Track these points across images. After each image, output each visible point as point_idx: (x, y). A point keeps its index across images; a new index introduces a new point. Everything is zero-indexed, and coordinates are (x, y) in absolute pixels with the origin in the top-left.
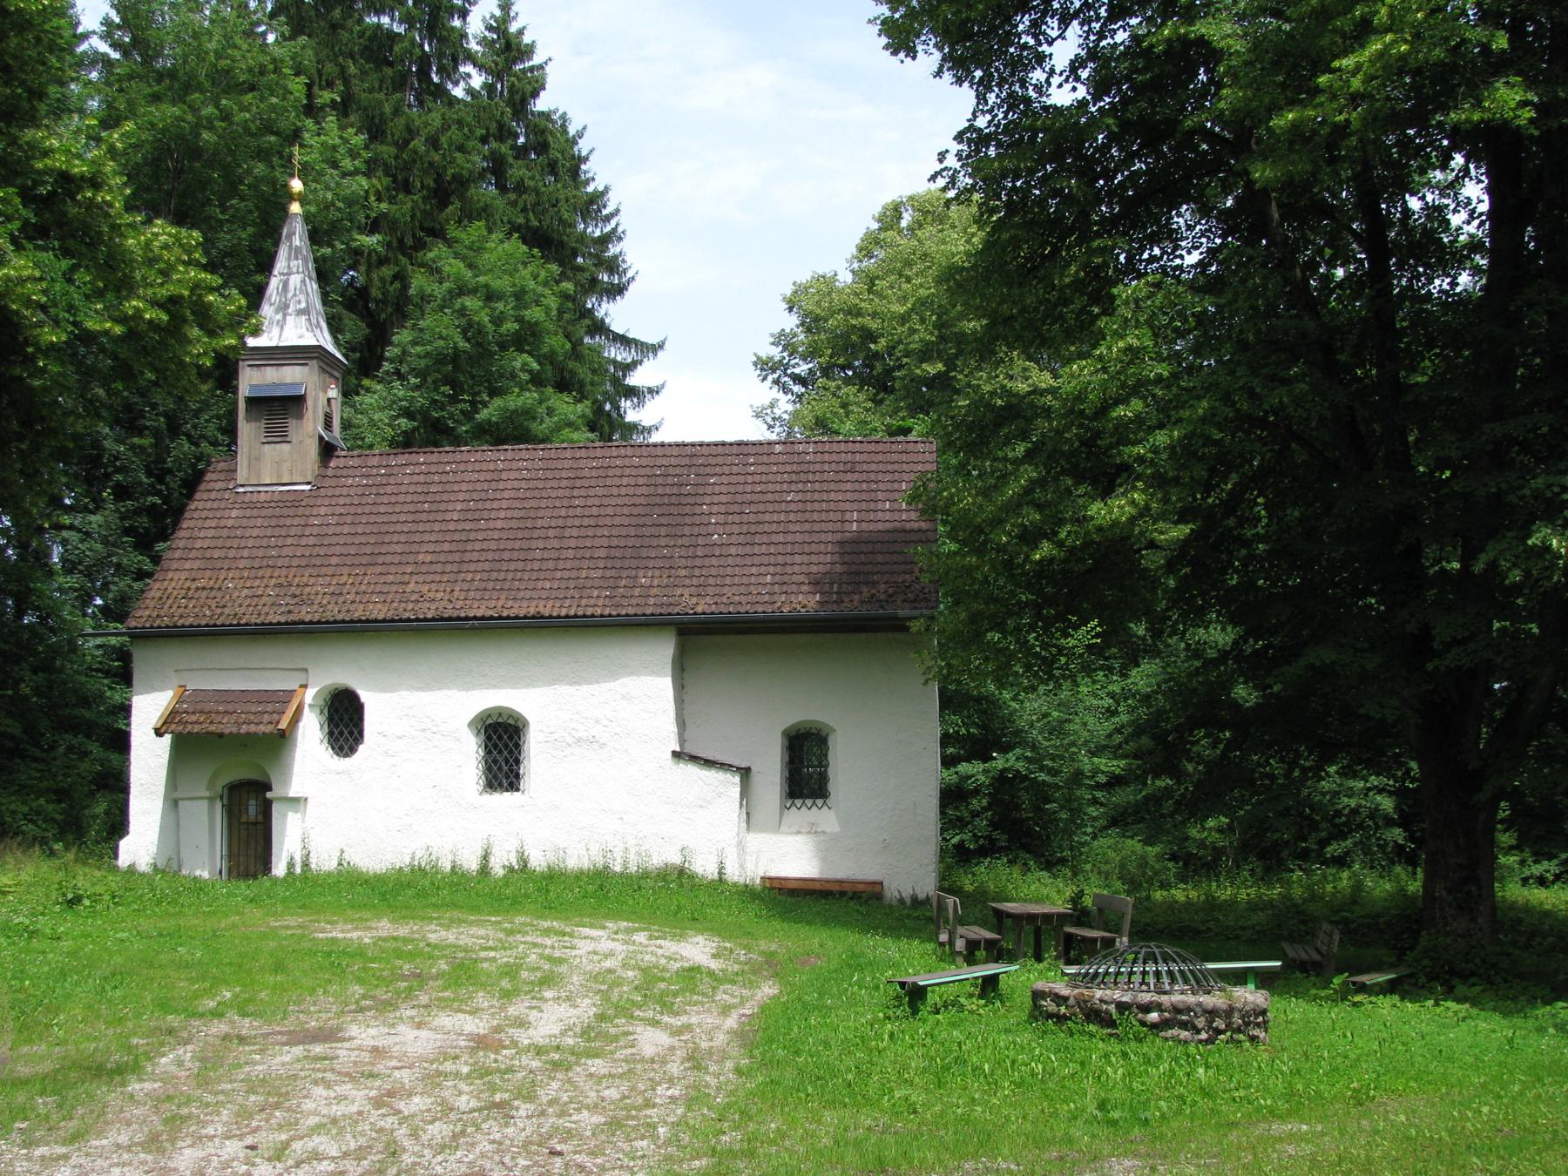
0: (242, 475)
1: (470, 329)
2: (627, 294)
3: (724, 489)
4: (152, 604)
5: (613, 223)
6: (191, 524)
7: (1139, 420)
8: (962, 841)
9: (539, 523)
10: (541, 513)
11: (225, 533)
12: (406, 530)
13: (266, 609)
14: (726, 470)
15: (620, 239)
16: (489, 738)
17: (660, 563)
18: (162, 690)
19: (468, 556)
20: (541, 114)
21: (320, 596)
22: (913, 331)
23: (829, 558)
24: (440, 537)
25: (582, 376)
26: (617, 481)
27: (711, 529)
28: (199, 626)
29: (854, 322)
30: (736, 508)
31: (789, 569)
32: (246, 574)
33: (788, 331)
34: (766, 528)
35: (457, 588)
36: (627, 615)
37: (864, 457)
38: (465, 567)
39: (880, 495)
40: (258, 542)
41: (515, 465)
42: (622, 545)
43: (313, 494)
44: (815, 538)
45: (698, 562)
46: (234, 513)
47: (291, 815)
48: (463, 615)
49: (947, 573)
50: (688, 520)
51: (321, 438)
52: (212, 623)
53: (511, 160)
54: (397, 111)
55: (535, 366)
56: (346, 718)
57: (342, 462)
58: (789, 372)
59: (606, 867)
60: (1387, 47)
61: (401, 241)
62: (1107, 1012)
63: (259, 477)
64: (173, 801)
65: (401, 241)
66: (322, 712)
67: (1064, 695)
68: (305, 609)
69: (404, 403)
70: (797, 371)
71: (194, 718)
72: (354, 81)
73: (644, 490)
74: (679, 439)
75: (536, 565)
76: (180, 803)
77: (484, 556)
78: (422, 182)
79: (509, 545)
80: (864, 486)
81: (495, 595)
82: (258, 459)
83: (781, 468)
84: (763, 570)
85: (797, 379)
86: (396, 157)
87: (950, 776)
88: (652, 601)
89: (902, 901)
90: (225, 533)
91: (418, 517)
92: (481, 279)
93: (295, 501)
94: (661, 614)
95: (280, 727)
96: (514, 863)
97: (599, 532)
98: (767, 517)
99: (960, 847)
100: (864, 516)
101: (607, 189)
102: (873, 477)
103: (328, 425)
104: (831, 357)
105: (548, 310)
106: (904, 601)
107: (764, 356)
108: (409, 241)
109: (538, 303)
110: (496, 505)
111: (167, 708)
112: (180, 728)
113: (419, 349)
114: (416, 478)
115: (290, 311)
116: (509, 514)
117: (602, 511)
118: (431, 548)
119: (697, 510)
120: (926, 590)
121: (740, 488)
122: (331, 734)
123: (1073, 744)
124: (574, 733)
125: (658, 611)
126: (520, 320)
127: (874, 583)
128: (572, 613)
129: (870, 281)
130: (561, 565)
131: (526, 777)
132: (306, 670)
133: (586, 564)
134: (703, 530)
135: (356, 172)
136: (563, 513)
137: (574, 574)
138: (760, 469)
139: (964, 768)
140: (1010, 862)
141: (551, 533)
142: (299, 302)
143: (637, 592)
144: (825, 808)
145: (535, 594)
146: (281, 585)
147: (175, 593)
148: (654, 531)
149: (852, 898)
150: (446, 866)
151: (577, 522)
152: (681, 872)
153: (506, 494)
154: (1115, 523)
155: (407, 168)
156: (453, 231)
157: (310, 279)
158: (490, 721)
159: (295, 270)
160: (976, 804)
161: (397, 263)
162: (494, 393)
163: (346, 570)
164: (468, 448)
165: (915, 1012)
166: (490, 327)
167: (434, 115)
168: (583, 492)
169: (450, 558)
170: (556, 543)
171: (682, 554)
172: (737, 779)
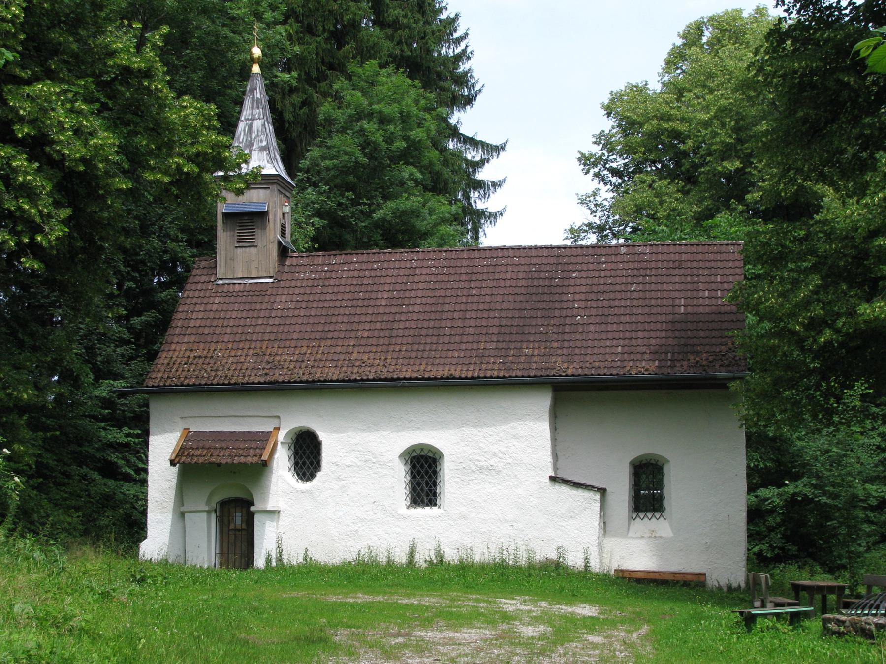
0: (221, 271)
1: (366, 145)
2: (476, 104)
3: (583, 281)
4: (163, 369)
6: (186, 308)
8: (761, 551)
9: (447, 308)
10: (447, 300)
11: (212, 315)
12: (347, 313)
13: (248, 372)
14: (585, 267)
15: (469, 58)
16: (413, 467)
17: (538, 338)
18: (171, 432)
19: (395, 333)
21: (287, 363)
22: (716, 134)
23: (664, 334)
25: (447, 176)
26: (502, 276)
27: (575, 312)
28: (200, 385)
29: (666, 126)
30: (593, 296)
31: (634, 342)
32: (230, 346)
33: (607, 132)
34: (616, 311)
35: (389, 357)
36: (516, 377)
37: (689, 257)
38: (393, 341)
39: (701, 286)
41: (425, 264)
42: (509, 324)
43: (275, 285)
44: (653, 318)
46: (217, 300)
47: (268, 523)
48: (395, 377)
49: (756, 349)
50: (557, 305)
51: (279, 243)
52: (209, 382)
55: (419, 176)
56: (301, 452)
58: (608, 166)
59: (503, 560)
61: (308, 74)
62: (870, 630)
63: (234, 273)
65: (308, 74)
66: (290, 448)
68: (277, 372)
69: (316, 205)
70: (614, 165)
71: (198, 452)
73: (523, 283)
75: (446, 340)
76: (186, 515)
77: (407, 333)
78: (324, 27)
79: (426, 324)
80: (689, 279)
81: (418, 362)
82: (232, 259)
83: (626, 266)
84: (615, 342)
85: (615, 172)
88: (534, 366)
89: (720, 588)
90: (212, 315)
91: (355, 303)
94: (541, 376)
95: (263, 458)
96: (433, 557)
97: (492, 314)
98: (617, 303)
99: (759, 555)
100: (689, 301)
101: (457, 16)
102: (695, 272)
103: (283, 234)
104: (644, 154)
105: (428, 131)
106: (721, 366)
108: (314, 74)
109: (420, 125)
110: (413, 294)
111: (177, 445)
112: (189, 459)
113: (328, 162)
114: (351, 274)
115: (254, 147)
116: (424, 301)
118: (367, 326)
119: (564, 298)
120: (737, 358)
121: (596, 281)
122: (296, 464)
123: (849, 474)
124: (477, 463)
125: (540, 373)
126: (406, 138)
127: (698, 352)
128: (476, 375)
129: (678, 91)
130: (465, 339)
131: (441, 496)
132: (279, 417)
133: (483, 338)
135: (276, 23)
137: (475, 346)
138: (611, 266)
140: (799, 567)
141: (456, 315)
142: (261, 141)
143: (522, 359)
144: (662, 519)
145: (447, 361)
146: (258, 354)
147: (179, 360)
149: (683, 585)
151: (475, 307)
153: (421, 286)
154: (876, 318)
156: (352, 67)
157: (268, 123)
158: (415, 454)
159: (257, 116)
160: (771, 521)
162: (386, 197)
163: (305, 343)
164: (389, 250)
165: (749, 630)
166: (384, 145)
168: (478, 284)
169: (382, 334)
170: (460, 323)
171: (555, 330)
172: (597, 497)
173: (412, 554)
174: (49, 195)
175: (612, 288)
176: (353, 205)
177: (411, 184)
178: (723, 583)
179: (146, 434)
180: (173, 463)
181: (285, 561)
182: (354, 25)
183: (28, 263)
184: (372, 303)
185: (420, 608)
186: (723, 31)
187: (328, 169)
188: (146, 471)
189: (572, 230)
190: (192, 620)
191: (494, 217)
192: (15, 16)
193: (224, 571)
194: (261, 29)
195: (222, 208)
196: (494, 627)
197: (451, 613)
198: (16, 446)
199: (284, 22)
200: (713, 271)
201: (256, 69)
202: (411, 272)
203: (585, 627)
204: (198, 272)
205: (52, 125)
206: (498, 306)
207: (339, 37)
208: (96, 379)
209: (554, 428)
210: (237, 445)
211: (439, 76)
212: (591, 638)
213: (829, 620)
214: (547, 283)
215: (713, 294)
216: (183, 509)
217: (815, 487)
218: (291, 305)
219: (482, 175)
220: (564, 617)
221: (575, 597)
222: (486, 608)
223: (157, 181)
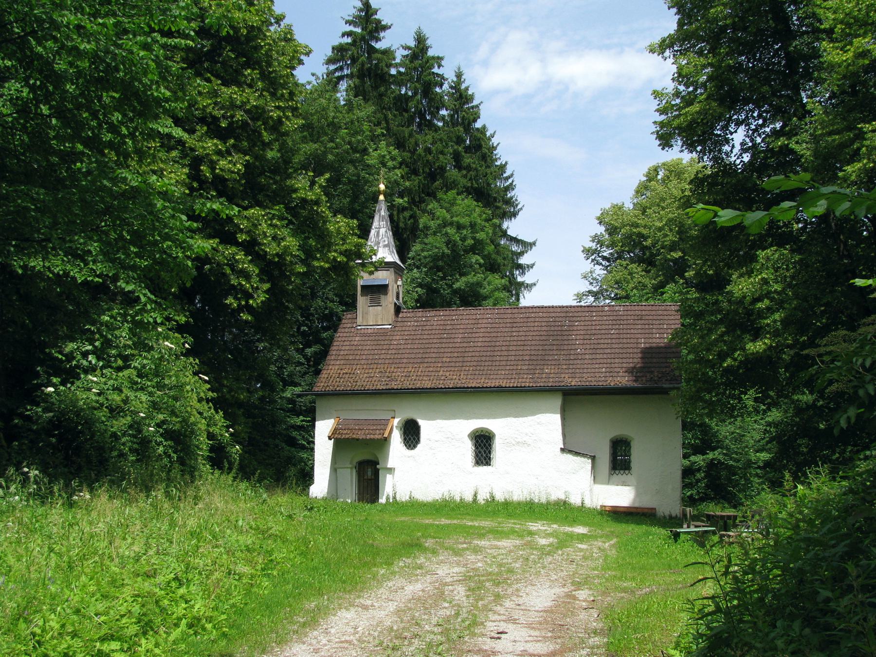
0: (359, 320)
2: (518, 217)
3: (582, 328)
5: (510, 181)
6: (338, 343)
7: (768, 309)
8: (692, 495)
9: (498, 344)
11: (354, 348)
14: (583, 319)
15: (513, 189)
16: (477, 442)
17: (554, 362)
20: (478, 129)
22: (666, 235)
24: (452, 350)
26: (532, 324)
27: (577, 347)
31: (613, 365)
34: (602, 346)
37: (647, 313)
38: (465, 364)
40: (369, 352)
45: (571, 362)
46: (357, 339)
50: (566, 342)
51: (395, 304)
53: (463, 154)
54: (411, 135)
55: (482, 261)
57: (405, 315)
59: (531, 500)
60: (865, 165)
61: (413, 199)
64: (335, 468)
65: (413, 199)
67: (738, 423)
72: (391, 122)
73: (545, 328)
74: (561, 304)
75: (497, 364)
77: (473, 359)
82: (367, 313)
83: (608, 318)
84: (601, 366)
85: (604, 258)
86: (411, 158)
87: (686, 463)
88: (551, 380)
89: (665, 517)
90: (354, 348)
92: (455, 219)
93: (384, 333)
97: (525, 348)
98: (602, 341)
99: (691, 497)
100: (647, 341)
102: (651, 322)
103: (398, 298)
105: (487, 233)
107: (587, 247)
109: (482, 230)
110: (477, 335)
113: (426, 253)
114: (439, 323)
116: (484, 339)
117: (526, 338)
118: (449, 355)
119: (570, 338)
122: (405, 439)
123: (747, 447)
126: (474, 238)
133: (520, 363)
134: (573, 347)
135: (394, 168)
136: (508, 339)
137: (515, 367)
138: (599, 318)
139: (693, 458)
141: (504, 348)
143: (544, 376)
145: (498, 377)
146: (381, 372)
148: (550, 347)
150: (458, 499)
151: (515, 343)
152: (565, 502)
153: (482, 330)
154: (757, 352)
155: (415, 162)
156: (440, 195)
160: (699, 476)
161: (411, 209)
162: (462, 275)
163: (410, 365)
165: (676, 541)
167: (428, 136)
168: (517, 329)
169: (458, 360)
170: (505, 353)
173: (475, 495)
174: (257, 275)
175: (599, 332)
176: (441, 280)
177: (477, 266)
178: (667, 513)
179: (313, 421)
180: (330, 438)
181: (398, 499)
182: (442, 169)
183: (245, 316)
184: (452, 341)
185: (479, 527)
186: (671, 172)
187: (425, 257)
188: (313, 443)
189: (578, 295)
190: (341, 532)
191: (529, 287)
192: (239, 170)
193: (361, 504)
194: (386, 173)
195: (360, 283)
196: (523, 539)
197: (497, 531)
198: (237, 427)
199: (400, 168)
200: (662, 322)
201: (382, 197)
202: (476, 321)
203: (578, 539)
204: (346, 321)
205: (259, 235)
206: (529, 343)
207: (432, 176)
208: (284, 386)
209: (563, 419)
210: (369, 427)
211: (495, 199)
212: (580, 546)
213: (724, 536)
214: (559, 328)
215: (662, 336)
216: (337, 466)
217: (725, 454)
218: (402, 342)
219: (522, 261)
220: (566, 534)
221: (574, 522)
222: (519, 528)
223: (321, 267)
